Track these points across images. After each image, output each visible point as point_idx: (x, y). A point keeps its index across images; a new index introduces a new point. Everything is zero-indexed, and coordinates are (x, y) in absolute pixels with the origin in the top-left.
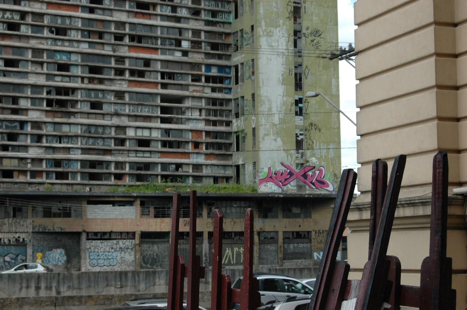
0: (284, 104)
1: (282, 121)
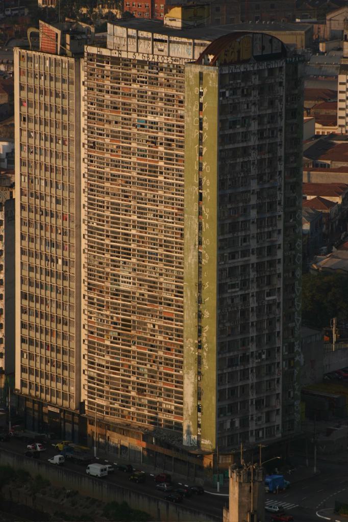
0: (193, 406)
1: (192, 414)
